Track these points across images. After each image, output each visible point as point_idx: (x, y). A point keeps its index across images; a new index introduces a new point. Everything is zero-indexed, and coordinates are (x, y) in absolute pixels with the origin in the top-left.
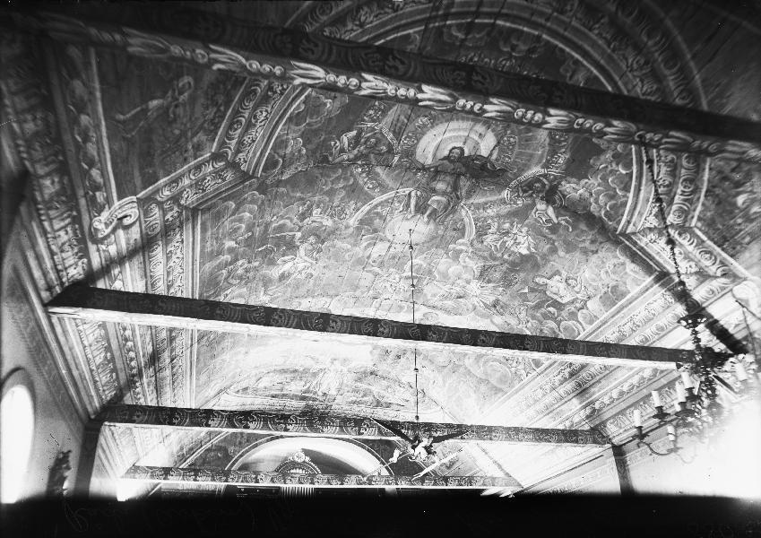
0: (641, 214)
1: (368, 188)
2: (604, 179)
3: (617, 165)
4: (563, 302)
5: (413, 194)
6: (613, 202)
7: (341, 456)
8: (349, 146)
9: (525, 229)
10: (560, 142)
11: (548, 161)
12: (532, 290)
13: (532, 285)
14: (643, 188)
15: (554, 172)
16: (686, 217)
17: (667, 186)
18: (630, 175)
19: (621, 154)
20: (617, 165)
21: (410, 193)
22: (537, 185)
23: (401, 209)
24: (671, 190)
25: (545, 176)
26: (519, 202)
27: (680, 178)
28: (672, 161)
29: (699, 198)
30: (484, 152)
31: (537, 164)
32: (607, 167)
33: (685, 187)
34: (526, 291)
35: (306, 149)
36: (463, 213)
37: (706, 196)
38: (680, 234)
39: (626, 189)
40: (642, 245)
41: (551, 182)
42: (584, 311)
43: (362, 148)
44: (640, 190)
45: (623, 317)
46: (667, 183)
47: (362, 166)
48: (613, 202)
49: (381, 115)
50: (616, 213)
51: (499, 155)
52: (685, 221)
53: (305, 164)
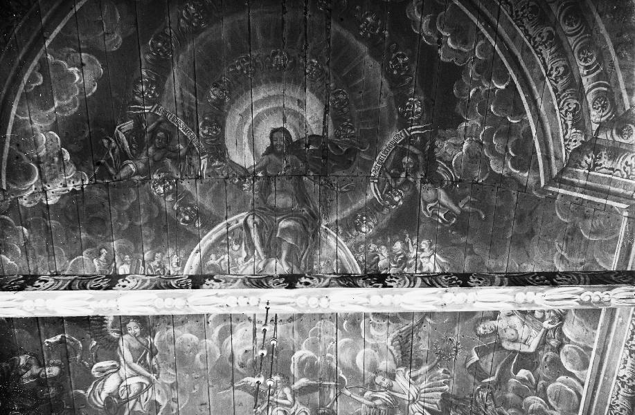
0: (555, 136)
1: (184, 221)
2: (484, 110)
3: (489, 80)
4: (532, 349)
5: (250, 223)
6: (514, 139)
7: (489, 290)
8: (131, 147)
9: (424, 244)
10: (402, 79)
11: (401, 115)
12: (482, 352)
13: (480, 343)
14: (538, 97)
15: (416, 129)
16: (612, 101)
17: (565, 73)
18: (512, 85)
19: (486, 62)
20: (489, 80)
21: (245, 221)
22: (406, 160)
23: (244, 254)
24: (572, 76)
25: (408, 140)
26: (396, 199)
27: (573, 52)
28: (551, 36)
29: (612, 66)
30: (315, 130)
31: (391, 127)
32: (478, 90)
33: (586, 61)
34: (475, 357)
35: (70, 151)
36: (333, 243)
37: (618, 54)
38: (620, 133)
39: (519, 111)
40: (583, 182)
41: (421, 147)
42: (566, 347)
43: (150, 150)
44: (535, 102)
45: (622, 324)
46: (562, 70)
47: (162, 182)
48: (514, 139)
49: (156, 91)
50: (526, 154)
51: (336, 127)
52: (614, 108)
53: (76, 178)
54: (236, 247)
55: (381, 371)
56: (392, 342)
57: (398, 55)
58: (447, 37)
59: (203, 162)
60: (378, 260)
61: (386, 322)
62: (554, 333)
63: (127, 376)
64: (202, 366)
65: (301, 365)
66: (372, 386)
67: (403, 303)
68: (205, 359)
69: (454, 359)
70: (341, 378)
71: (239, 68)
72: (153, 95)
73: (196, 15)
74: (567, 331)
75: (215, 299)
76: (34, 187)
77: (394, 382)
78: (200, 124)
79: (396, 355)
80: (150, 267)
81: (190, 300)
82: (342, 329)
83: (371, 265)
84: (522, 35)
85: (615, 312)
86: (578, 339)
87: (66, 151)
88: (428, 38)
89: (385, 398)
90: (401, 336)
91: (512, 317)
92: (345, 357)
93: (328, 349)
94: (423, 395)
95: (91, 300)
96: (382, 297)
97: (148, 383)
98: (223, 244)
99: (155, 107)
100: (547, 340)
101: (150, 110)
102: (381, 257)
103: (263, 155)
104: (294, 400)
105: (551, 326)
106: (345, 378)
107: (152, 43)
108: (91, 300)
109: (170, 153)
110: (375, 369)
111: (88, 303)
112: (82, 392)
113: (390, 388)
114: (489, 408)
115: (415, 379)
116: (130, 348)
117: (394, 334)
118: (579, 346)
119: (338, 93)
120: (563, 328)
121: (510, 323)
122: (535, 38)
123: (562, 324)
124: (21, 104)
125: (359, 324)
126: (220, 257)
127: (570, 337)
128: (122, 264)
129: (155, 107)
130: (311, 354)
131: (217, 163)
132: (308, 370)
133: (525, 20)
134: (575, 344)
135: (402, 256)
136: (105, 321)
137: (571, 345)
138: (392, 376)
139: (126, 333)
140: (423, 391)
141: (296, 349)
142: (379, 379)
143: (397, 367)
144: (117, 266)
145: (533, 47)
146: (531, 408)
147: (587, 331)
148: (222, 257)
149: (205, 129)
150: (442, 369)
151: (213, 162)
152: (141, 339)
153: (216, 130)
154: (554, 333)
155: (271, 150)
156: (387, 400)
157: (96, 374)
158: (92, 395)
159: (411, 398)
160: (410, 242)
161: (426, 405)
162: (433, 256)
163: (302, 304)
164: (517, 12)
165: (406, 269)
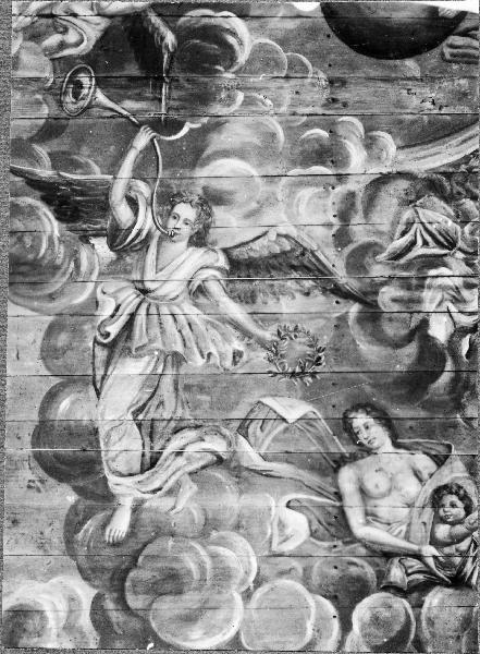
55: (210, 215)
61: (335, 221)
62: (419, 572)
65: (214, 34)
66: (167, 199)
69: (275, 370)
70: (180, 126)
74: (434, 599)
77: (185, 243)
79: (256, 246)
82: (307, 126)
83: (462, 185)
85: (311, 572)
86: (431, 622)
89: (137, 227)
90: (303, 254)
91: (414, 480)
92: (237, 133)
93: (255, 94)
94: (164, 310)
100: (396, 560)
105: (431, 562)
106: (173, 138)
110: (211, 199)
113: (168, 237)
114: (181, 461)
117: (306, 238)
118: (418, 627)
120: (437, 588)
121: (400, 477)
123: (448, 586)
125: (323, 163)
127: (426, 605)
130: (242, 57)
132: (197, 50)
134: (418, 619)
137: (410, 611)
138: (199, 240)
140: (177, 310)
141: (255, 23)
142: (185, 211)
143: (225, 251)
146: (221, 550)
147: (458, 637)
150: (241, 348)
154: (419, 572)
156: (134, 232)
159: (149, 285)
161: (141, 318)
165: (460, 255)
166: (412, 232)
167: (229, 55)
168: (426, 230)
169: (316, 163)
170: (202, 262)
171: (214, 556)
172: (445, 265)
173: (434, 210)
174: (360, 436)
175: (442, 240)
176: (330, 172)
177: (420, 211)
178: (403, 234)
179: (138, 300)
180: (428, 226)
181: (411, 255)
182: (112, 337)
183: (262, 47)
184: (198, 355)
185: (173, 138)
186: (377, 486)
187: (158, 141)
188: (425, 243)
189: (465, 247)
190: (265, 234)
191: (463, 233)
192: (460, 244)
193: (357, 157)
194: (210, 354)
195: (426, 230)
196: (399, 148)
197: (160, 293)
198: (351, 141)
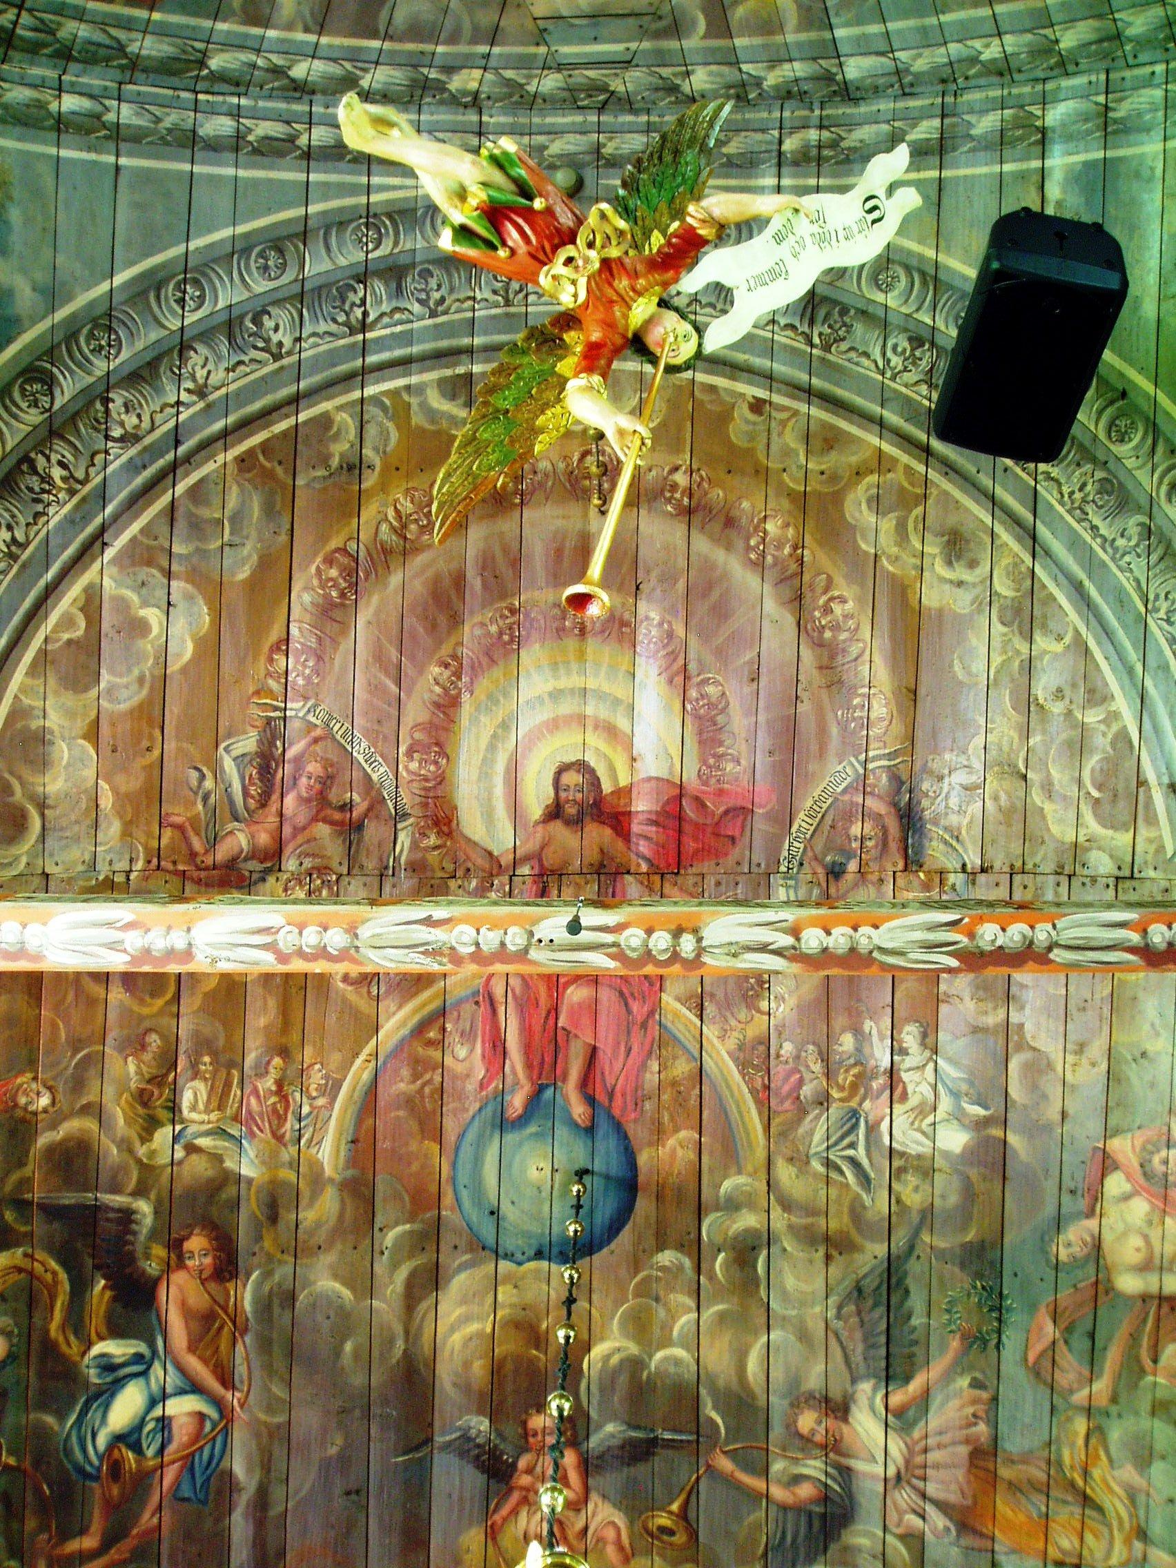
8: (246, 793)
54: (462, 1052)
56: (840, 1308)
57: (832, 599)
58: (934, 557)
59: (402, 837)
60: (801, 1082)
63: (169, 1390)
64: (358, 1380)
65: (609, 1379)
67: (880, 949)
68: (366, 1359)
71: (494, 629)
72: (308, 679)
73: (415, 517)
75: (424, 934)
76: (24, 860)
77: (845, 1428)
78: (402, 749)
80: (255, 1092)
81: (365, 932)
82: (712, 1277)
84: (1088, 539)
87: (106, 787)
88: (895, 560)
92: (717, 1357)
95: (130, 926)
96: (828, 933)
97: (214, 1415)
98: (430, 1043)
99: (310, 704)
101: (298, 710)
102: (807, 1076)
103: (537, 823)
104: (587, 1490)
106: (719, 1421)
107: (318, 568)
108: (130, 926)
109: (329, 812)
111: (119, 935)
112: (50, 1420)
115: (900, 1413)
116: (187, 1312)
119: (705, 682)
122: (1114, 540)
124: (32, 671)
126: (422, 1075)
128: (193, 1079)
129: (310, 704)
130: (633, 1349)
131: (433, 840)
133: (1090, 509)
135: (855, 1071)
136: (134, 1226)
138: (838, 1408)
139: (181, 1265)
144: (180, 1081)
145: (1113, 559)
148: (427, 1077)
149: (412, 759)
151: (424, 835)
152: (212, 1286)
153: (436, 763)
155: (555, 812)
157: (94, 1376)
158: (74, 1433)
159: (892, 1471)
160: (874, 1032)
162: (931, 1066)
163: (634, 950)
164: (1071, 493)
165: (867, 1105)
166: (839, 1162)
167: (635, 1365)
168: (836, 1144)
169: (755, 1268)
170: (866, 1409)
171: (946, 829)
172: (878, 1123)
173: (811, 1133)
174: (1079, 1255)
175: (848, 1125)
176: (765, 1252)
177: (812, 1151)
178: (842, 1173)
179: (908, 1489)
180: (831, 1141)
181: (865, 1162)
182: (949, 1524)
183: (623, 1324)
184: (974, 1429)
185: (719, 1421)
186: (1138, 1250)
187: (727, 1444)
188: (852, 1145)
189: (857, 1099)
190: (837, 1335)
191: (841, 1100)
192: (853, 1104)
193: (748, 1220)
194: (974, 1415)
195: (836, 1144)
196: (739, 1172)
197: (900, 1461)
198: (728, 1228)
